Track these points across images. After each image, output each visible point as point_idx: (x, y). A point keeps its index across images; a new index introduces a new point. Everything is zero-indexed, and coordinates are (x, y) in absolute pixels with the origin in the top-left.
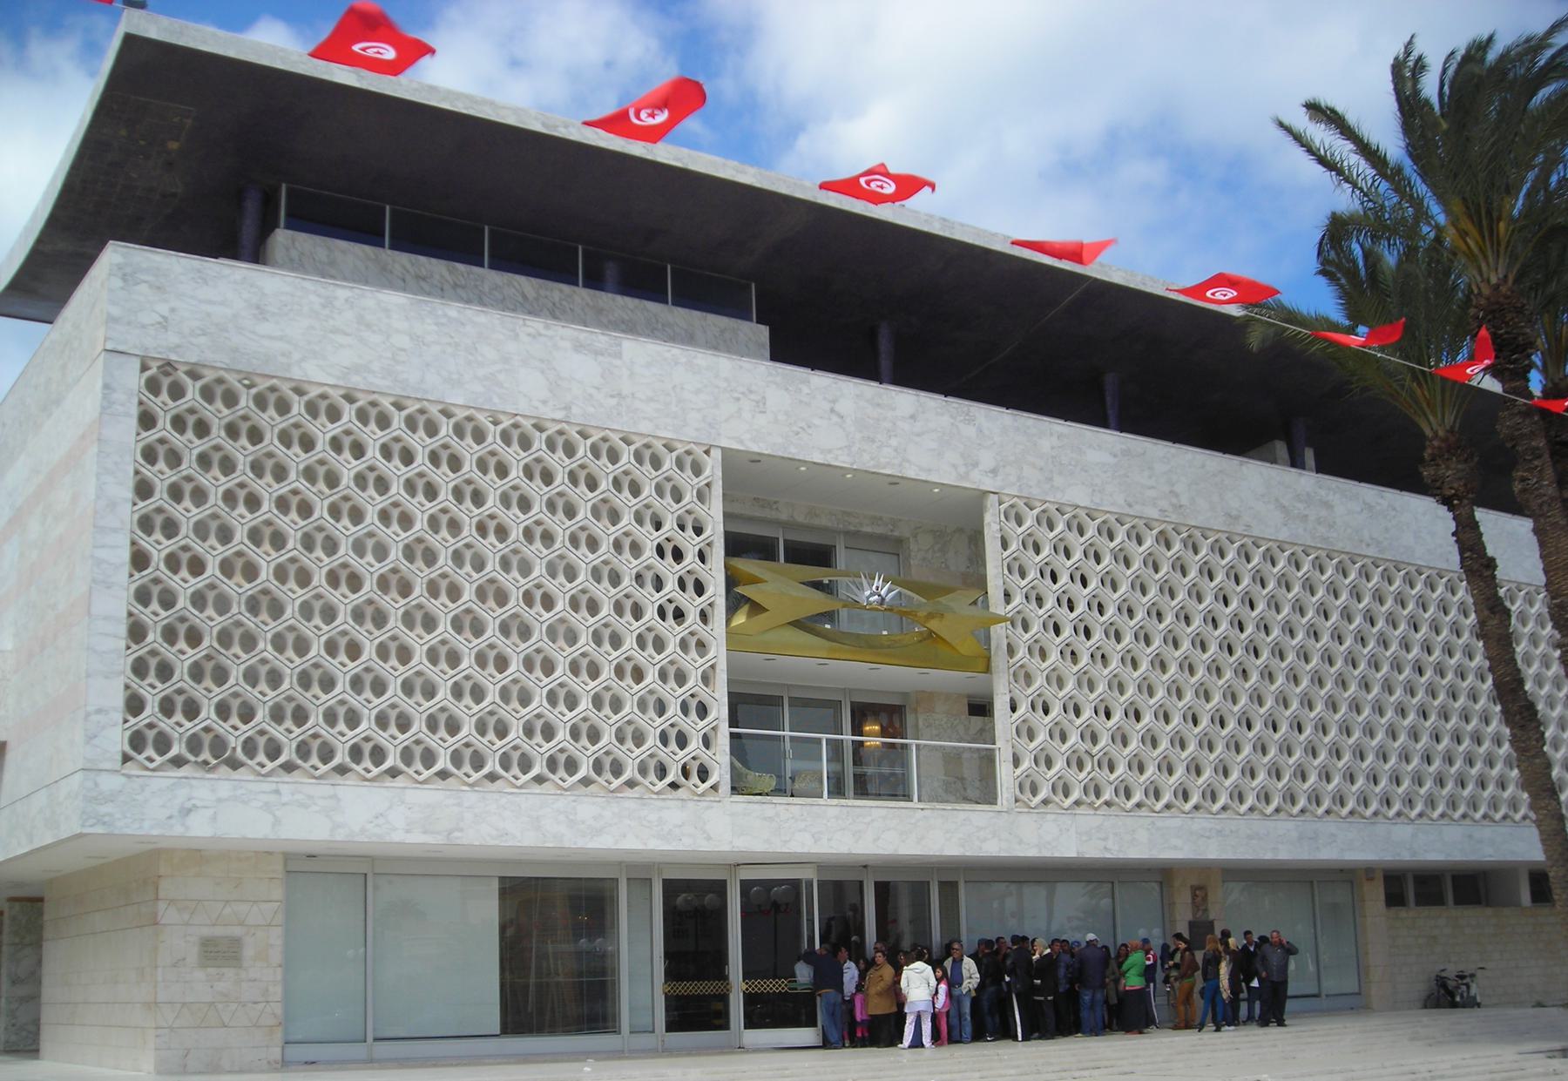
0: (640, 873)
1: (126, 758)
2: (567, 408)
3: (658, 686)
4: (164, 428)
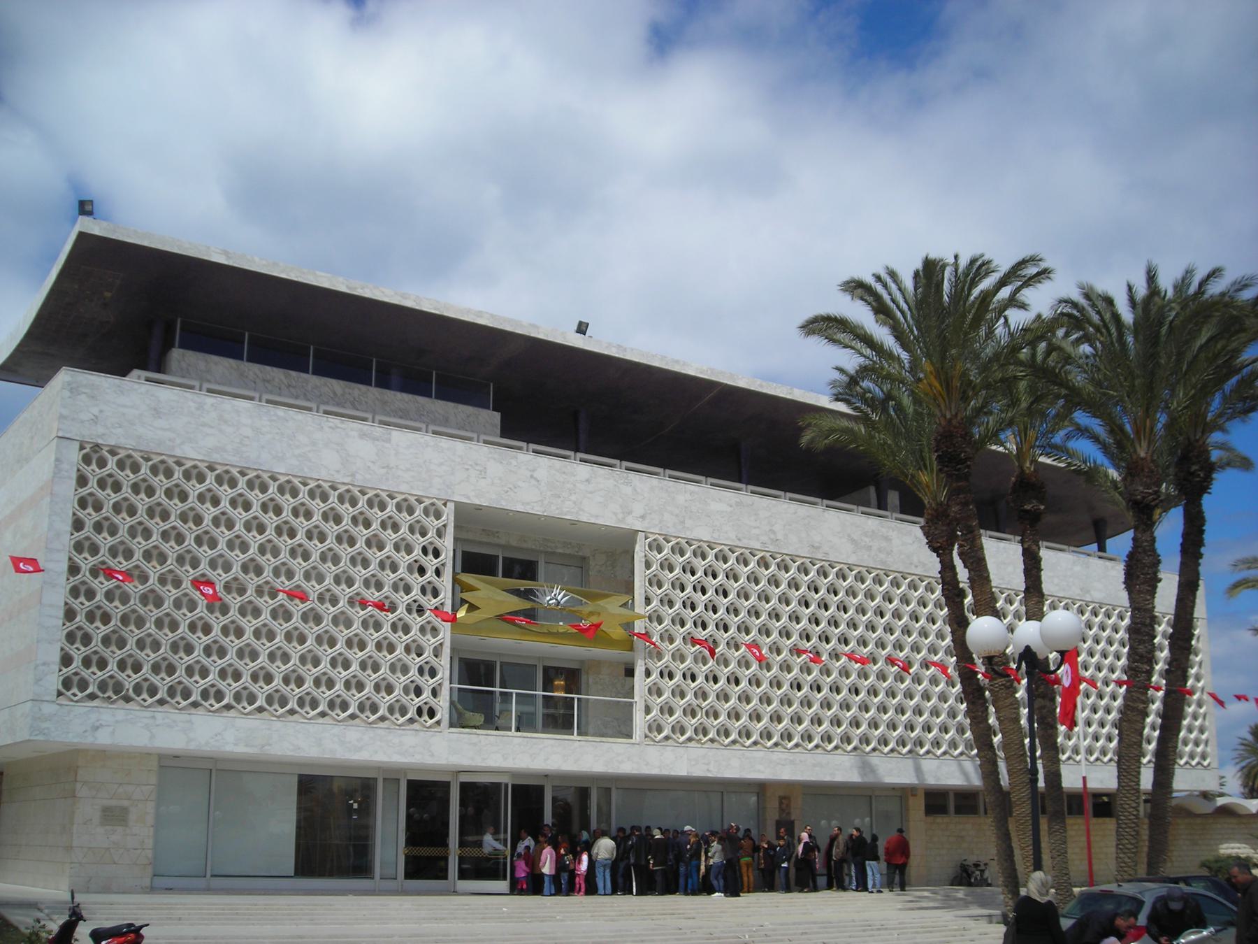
0: (391, 776)
1: (60, 694)
2: (353, 475)
3: (404, 656)
4: (92, 486)
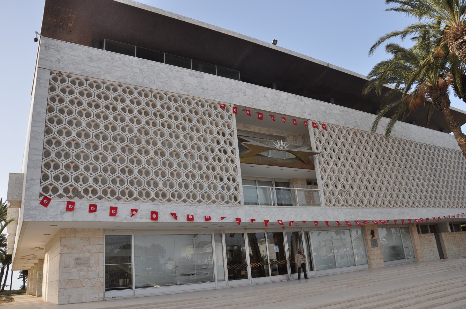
2: (188, 91)
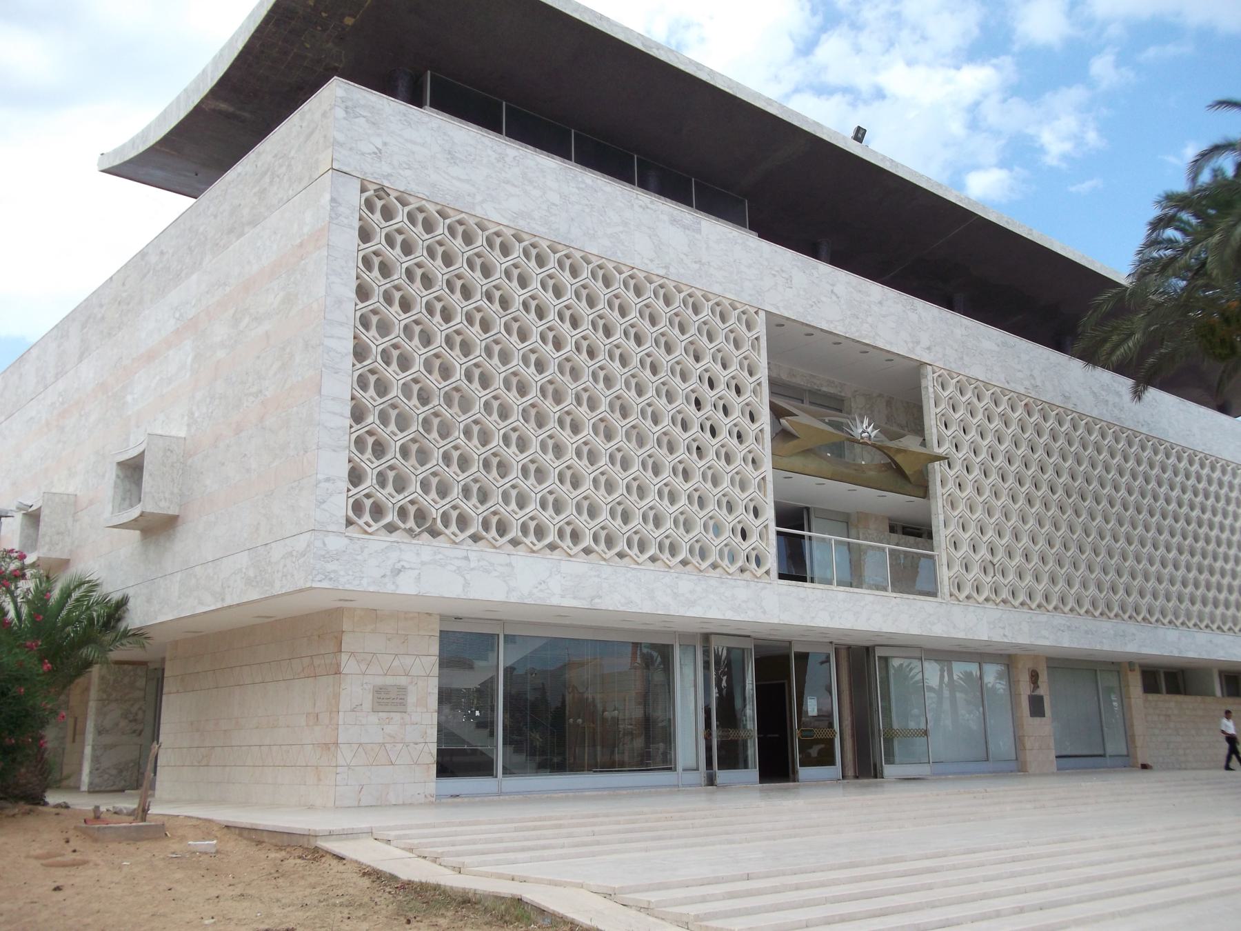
2: (666, 267)
